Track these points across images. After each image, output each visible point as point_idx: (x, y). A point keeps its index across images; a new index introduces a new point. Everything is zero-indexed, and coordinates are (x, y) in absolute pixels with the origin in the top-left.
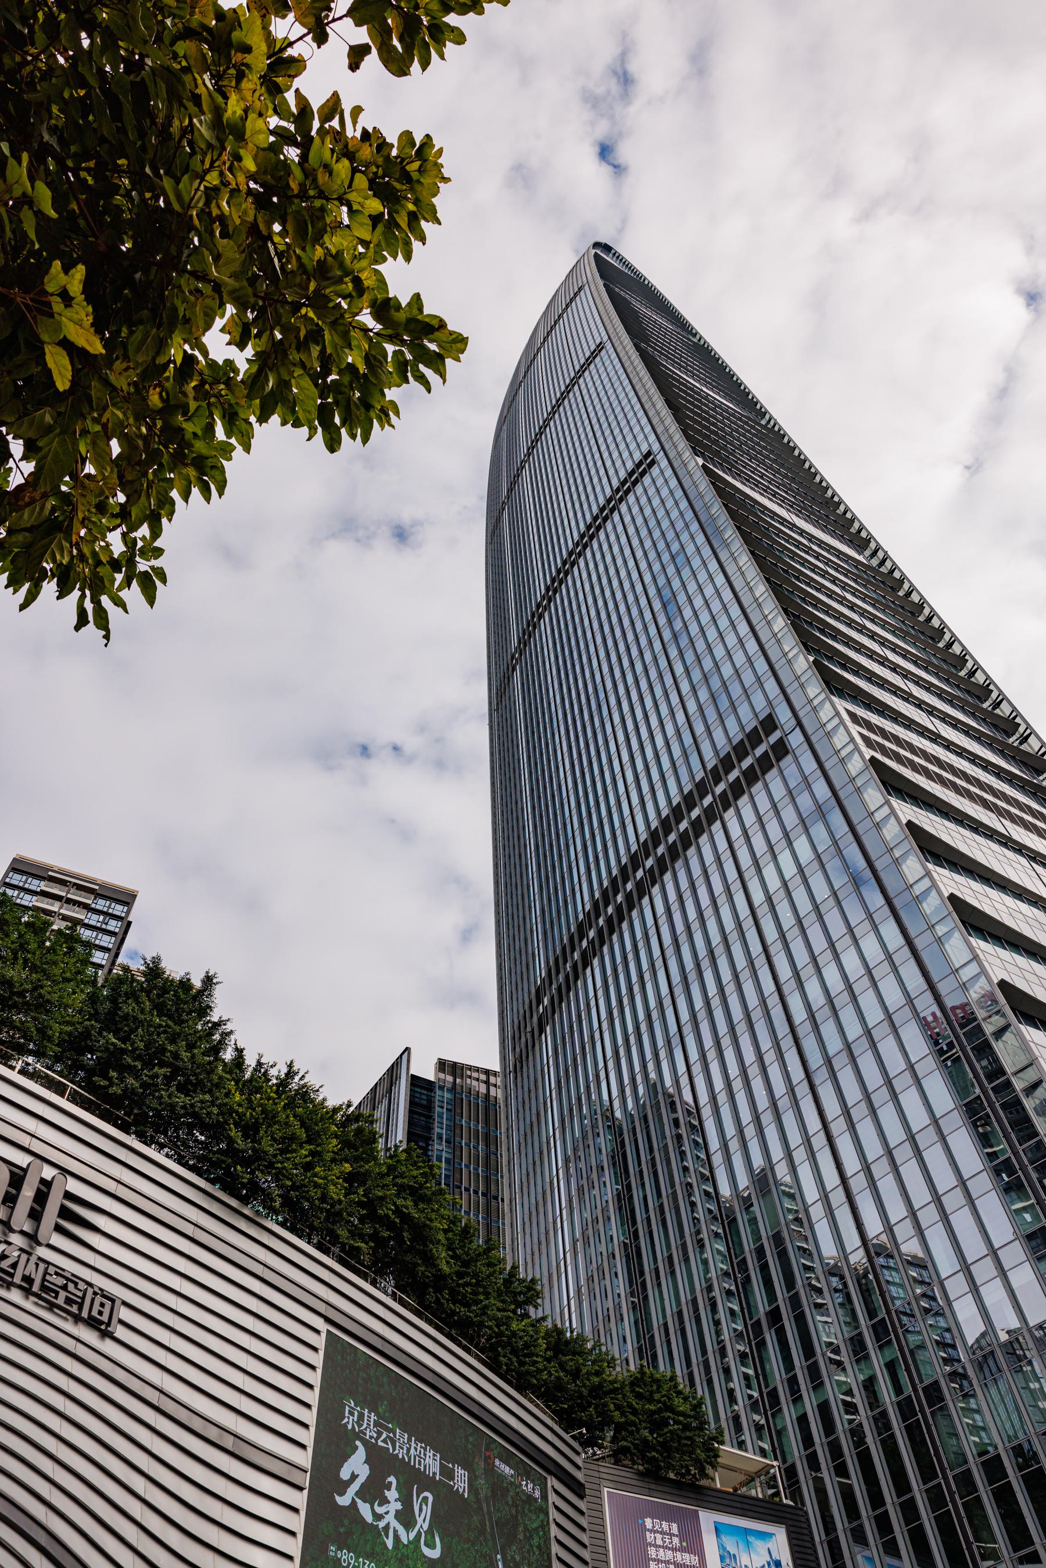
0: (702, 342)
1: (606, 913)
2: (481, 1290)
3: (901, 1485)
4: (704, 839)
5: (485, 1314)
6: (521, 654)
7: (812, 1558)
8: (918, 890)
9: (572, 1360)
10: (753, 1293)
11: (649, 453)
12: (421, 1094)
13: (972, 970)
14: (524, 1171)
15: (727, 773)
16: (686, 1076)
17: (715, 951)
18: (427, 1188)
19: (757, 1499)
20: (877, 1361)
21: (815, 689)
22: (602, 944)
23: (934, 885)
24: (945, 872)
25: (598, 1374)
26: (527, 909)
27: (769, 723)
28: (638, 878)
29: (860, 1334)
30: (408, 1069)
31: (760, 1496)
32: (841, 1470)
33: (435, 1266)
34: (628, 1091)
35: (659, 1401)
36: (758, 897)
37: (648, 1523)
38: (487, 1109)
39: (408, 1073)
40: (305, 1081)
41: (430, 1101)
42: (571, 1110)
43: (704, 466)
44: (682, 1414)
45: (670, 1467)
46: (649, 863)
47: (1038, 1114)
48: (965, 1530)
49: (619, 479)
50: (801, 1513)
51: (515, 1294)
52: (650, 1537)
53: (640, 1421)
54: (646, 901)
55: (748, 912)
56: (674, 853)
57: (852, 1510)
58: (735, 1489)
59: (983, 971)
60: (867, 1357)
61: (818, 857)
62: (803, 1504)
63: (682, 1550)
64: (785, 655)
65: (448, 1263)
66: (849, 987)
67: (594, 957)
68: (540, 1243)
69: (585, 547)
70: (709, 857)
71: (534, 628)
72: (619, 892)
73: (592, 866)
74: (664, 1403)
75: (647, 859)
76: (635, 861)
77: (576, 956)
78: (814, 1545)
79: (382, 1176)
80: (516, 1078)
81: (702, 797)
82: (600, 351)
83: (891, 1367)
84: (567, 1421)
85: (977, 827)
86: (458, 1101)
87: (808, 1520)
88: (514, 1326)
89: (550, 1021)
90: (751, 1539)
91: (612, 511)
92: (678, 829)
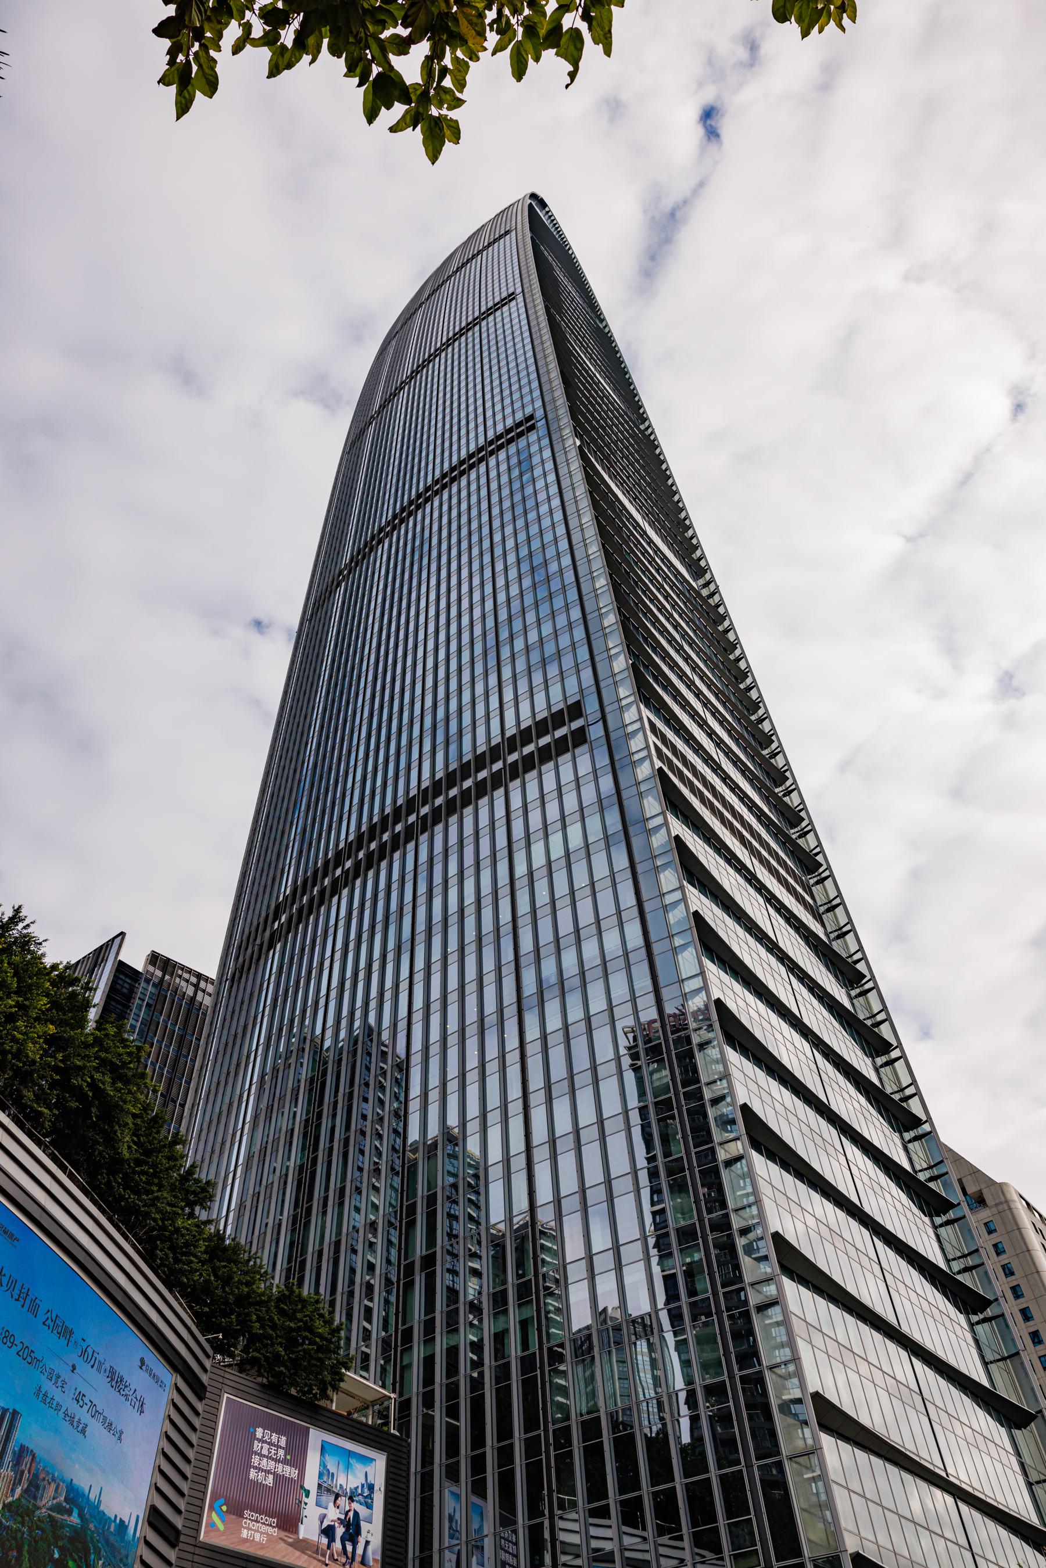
0: (606, 330)
1: (368, 847)
2: (156, 1181)
3: (504, 1431)
4: (484, 802)
5: (154, 1205)
6: (349, 573)
7: (403, 1486)
8: (669, 899)
9: (225, 1267)
10: (414, 1237)
11: (531, 417)
12: (125, 981)
13: (697, 983)
14: (215, 1080)
15: (523, 745)
16: (405, 1021)
17: (466, 910)
18: (129, 1068)
19: (366, 1425)
20: (514, 1316)
21: (626, 691)
22: (356, 877)
23: (684, 899)
24: (695, 891)
25: (248, 1284)
26: (288, 824)
27: (576, 710)
28: (410, 822)
29: (505, 1291)
30: (118, 954)
31: (370, 1423)
32: (453, 1411)
33: (114, 1148)
34: (344, 1023)
35: (301, 1320)
36: (521, 869)
37: (259, 1433)
38: (189, 1012)
39: (116, 957)
40: (29, 930)
41: (132, 991)
42: (281, 1030)
43: (580, 447)
44: (320, 1336)
45: (295, 1384)
46: (425, 810)
47: (717, 1126)
48: (550, 1477)
49: (495, 432)
50: (404, 1444)
51: (187, 1192)
52: (257, 1446)
53: (277, 1336)
54: (411, 846)
55: (507, 881)
56: (451, 807)
57: (452, 1447)
58: (349, 1413)
59: (705, 987)
60: (505, 1312)
61: (587, 846)
62: (408, 1435)
63: (285, 1462)
64: (608, 650)
65: (129, 1147)
66: (582, 973)
67: (345, 887)
68: (213, 1152)
69: (444, 487)
70: (484, 820)
71: (371, 550)
72: (387, 830)
73: (367, 799)
74: (305, 1323)
75: (423, 806)
76: (411, 805)
77: (326, 882)
78: (409, 1475)
79: (86, 1045)
80: (231, 987)
81: (493, 762)
82: (510, 301)
83: (524, 1324)
84: (205, 1323)
85: (731, 859)
86: (161, 998)
87: (409, 1452)
88: (179, 1222)
89: (283, 939)
90: (352, 1461)
91: (480, 460)
92: (461, 786)
